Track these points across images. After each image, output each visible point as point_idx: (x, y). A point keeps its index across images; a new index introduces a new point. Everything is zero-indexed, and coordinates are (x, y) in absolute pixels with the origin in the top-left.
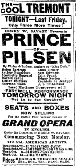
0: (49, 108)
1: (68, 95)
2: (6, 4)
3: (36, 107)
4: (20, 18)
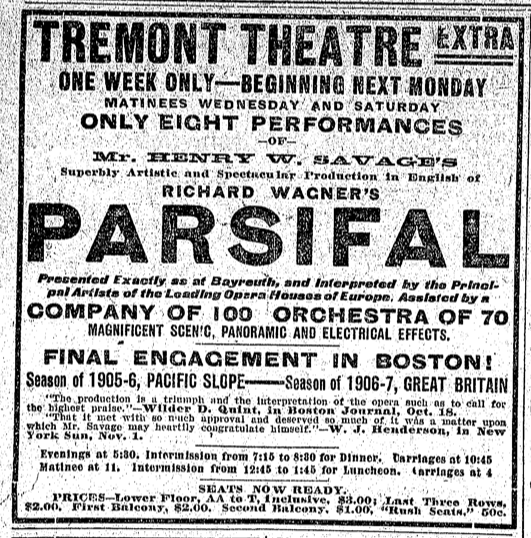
0: (392, 361)
1: (224, 123)
3: (324, 103)
4: (271, 80)
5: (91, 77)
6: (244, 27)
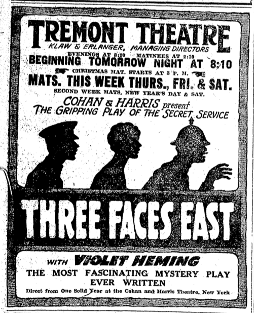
5: (225, 32)
6: (138, 25)
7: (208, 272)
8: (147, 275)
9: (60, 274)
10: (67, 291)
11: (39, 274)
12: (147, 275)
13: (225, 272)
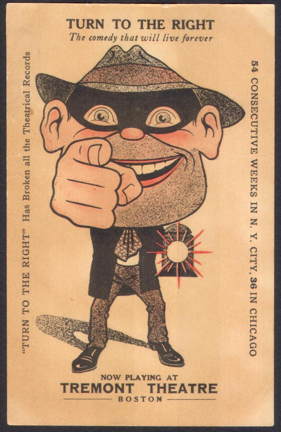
2: (159, 385)
7: (126, 376)
8: (160, 379)
9: (185, 26)
10: (26, 284)
11: (157, 27)
12: (160, 379)
13: (143, 376)
